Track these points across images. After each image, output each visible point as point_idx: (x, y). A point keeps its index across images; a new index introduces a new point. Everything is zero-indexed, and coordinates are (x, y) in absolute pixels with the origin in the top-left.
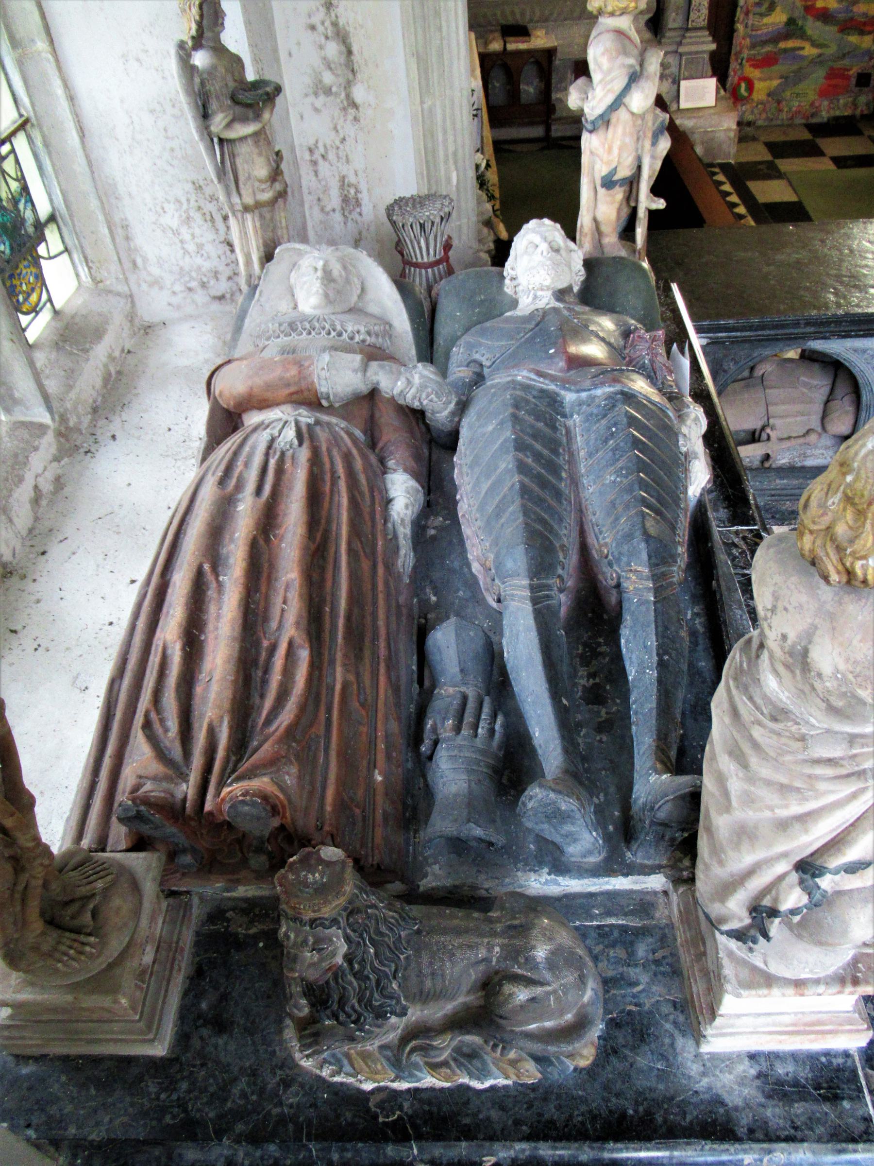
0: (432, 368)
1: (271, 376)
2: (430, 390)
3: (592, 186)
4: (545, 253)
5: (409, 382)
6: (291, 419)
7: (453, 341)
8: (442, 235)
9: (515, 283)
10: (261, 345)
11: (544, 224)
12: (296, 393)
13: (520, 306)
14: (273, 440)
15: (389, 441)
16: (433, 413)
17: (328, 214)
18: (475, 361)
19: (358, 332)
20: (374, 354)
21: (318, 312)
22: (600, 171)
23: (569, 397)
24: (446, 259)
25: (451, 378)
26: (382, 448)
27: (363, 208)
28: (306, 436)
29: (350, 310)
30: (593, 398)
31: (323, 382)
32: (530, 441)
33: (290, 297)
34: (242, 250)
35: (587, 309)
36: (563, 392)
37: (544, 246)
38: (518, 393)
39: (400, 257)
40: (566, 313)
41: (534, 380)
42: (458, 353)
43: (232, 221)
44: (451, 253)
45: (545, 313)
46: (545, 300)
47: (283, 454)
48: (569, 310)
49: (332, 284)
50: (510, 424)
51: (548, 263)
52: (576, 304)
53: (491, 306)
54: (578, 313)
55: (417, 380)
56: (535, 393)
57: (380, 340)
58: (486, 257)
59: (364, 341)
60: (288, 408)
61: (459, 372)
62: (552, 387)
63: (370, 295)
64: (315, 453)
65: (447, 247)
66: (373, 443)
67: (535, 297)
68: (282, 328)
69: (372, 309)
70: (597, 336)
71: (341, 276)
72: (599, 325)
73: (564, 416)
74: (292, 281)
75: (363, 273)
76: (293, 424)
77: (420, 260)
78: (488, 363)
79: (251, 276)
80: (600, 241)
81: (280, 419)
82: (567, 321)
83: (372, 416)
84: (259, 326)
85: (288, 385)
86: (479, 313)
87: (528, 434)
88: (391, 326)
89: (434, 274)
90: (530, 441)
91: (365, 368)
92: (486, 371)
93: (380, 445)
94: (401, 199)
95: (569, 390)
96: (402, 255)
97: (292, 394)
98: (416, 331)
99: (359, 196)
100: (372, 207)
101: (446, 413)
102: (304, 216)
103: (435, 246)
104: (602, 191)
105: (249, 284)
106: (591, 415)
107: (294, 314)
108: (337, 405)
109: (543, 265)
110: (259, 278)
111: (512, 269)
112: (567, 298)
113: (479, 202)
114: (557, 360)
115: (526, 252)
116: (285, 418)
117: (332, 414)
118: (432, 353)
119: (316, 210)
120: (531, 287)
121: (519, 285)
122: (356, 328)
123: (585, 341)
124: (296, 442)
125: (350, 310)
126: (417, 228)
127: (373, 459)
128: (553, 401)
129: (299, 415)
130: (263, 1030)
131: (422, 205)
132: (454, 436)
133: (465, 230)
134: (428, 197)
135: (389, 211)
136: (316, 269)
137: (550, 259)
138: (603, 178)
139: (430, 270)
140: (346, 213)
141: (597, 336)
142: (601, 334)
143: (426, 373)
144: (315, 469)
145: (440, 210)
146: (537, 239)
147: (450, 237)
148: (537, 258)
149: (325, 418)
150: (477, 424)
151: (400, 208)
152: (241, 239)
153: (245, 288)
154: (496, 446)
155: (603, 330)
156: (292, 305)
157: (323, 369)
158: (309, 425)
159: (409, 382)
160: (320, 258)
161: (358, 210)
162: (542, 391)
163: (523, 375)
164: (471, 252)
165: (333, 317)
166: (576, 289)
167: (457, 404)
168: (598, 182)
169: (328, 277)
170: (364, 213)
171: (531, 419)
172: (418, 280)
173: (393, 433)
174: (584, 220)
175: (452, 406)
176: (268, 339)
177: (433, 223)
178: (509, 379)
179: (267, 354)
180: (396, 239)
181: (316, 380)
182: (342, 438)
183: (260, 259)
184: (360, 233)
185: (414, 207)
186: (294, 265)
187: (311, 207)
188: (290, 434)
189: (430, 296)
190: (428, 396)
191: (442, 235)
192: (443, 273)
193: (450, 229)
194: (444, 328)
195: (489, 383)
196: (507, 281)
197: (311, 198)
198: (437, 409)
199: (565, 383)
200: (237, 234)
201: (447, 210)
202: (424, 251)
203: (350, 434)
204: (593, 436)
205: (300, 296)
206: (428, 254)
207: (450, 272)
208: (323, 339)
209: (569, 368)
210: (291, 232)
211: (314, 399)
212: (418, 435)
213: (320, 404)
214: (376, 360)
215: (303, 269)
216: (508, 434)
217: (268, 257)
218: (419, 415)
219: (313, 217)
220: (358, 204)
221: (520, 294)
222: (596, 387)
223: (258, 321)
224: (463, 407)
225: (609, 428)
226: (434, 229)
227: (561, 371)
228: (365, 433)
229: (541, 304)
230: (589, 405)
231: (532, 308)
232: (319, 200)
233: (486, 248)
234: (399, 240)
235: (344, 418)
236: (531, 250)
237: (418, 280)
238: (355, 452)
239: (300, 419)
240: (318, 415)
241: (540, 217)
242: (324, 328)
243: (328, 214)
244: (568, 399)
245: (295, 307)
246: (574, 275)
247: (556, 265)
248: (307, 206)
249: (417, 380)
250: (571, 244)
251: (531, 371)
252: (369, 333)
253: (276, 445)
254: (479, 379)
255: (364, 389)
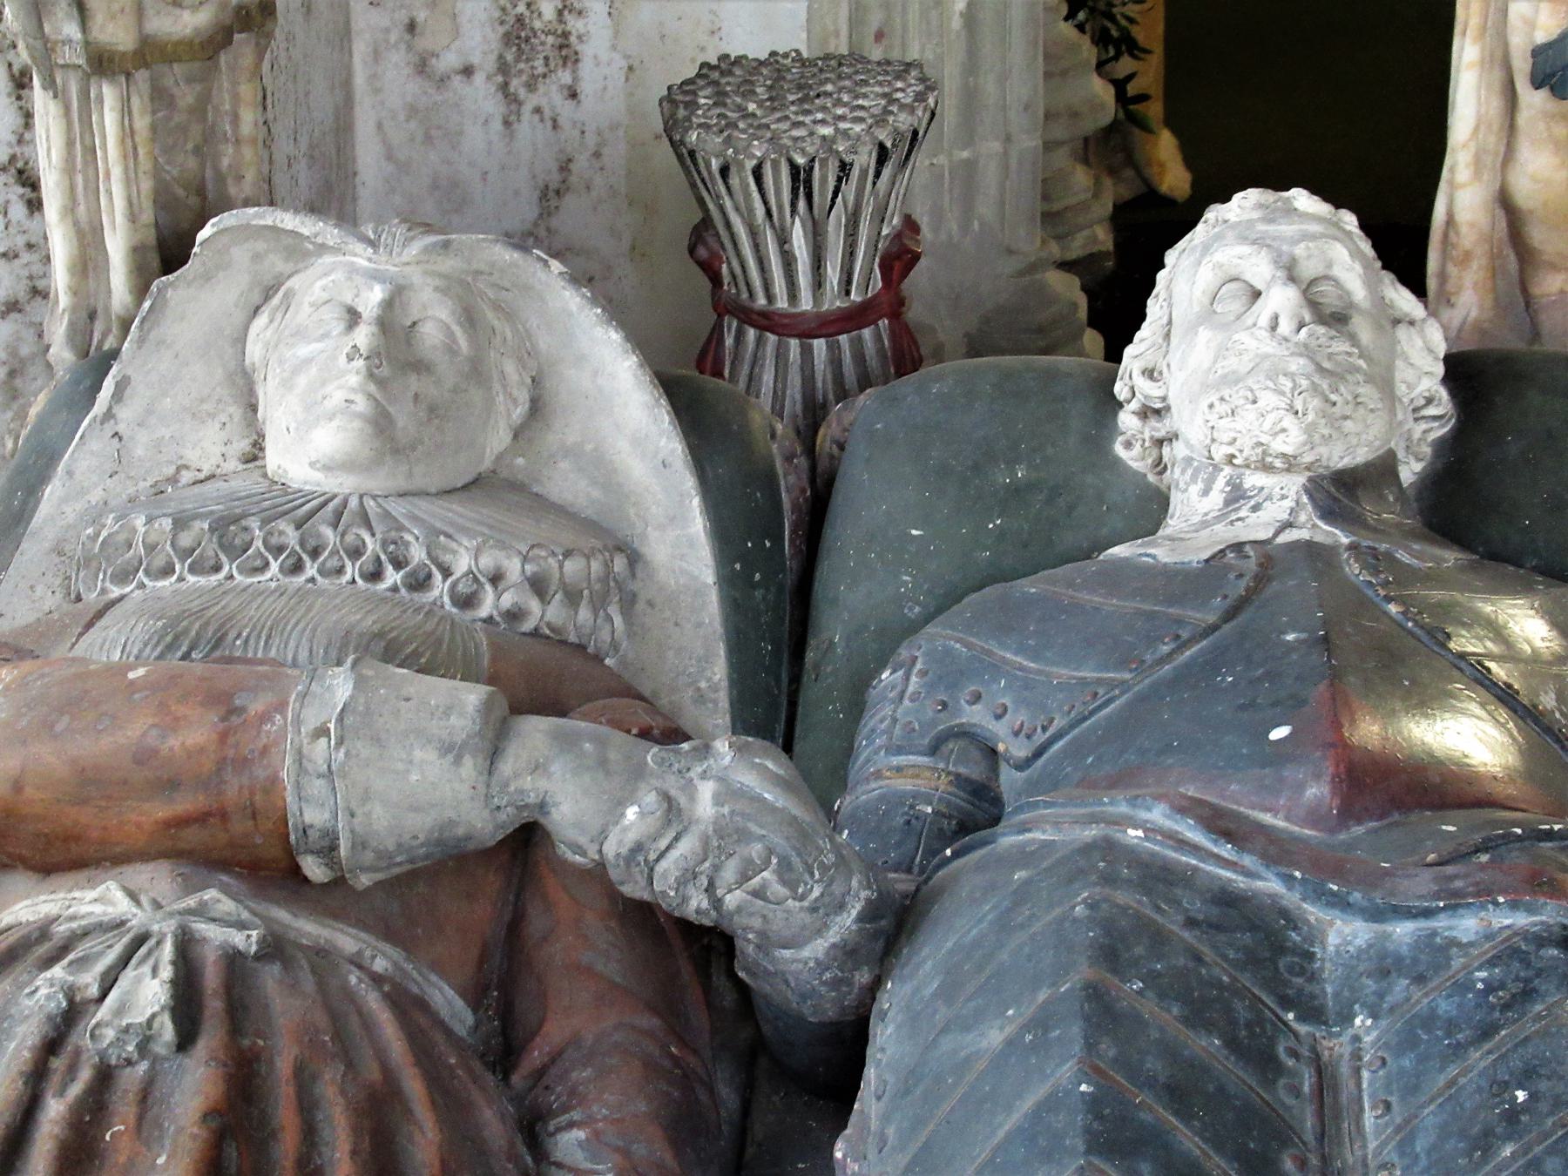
0: (774, 763)
1: (106, 742)
2: (756, 850)
3: (1498, 75)
4: (1285, 327)
5: (673, 812)
6: (166, 928)
7: (887, 642)
8: (880, 217)
9: (1160, 428)
10: (91, 597)
11: (1291, 211)
12: (202, 818)
13: (1174, 524)
14: (72, 1013)
15: (575, 1041)
16: (766, 942)
17: (443, 81)
18: (963, 732)
19: (496, 579)
20: (543, 680)
21: (341, 484)
22: (1531, 25)
23: (1342, 934)
24: (890, 304)
25: (860, 796)
26: (540, 1073)
27: (586, 67)
28: (214, 1005)
29: (477, 486)
30: (1437, 951)
31: (317, 787)
32: (1154, 1111)
33: (236, 411)
34: (70, 209)
35: (1451, 557)
36: (1313, 912)
37: (1282, 299)
38: (1122, 897)
39: (705, 283)
40: (1353, 570)
41: (1195, 849)
42: (900, 695)
43: (39, 97)
44: (918, 281)
45: (1270, 562)
46: (1276, 511)
47: (105, 1076)
48: (1374, 560)
49: (414, 382)
50: (1076, 1030)
51: (1298, 364)
52: (1414, 535)
53: (1061, 503)
54: (1406, 576)
55: (705, 803)
56: (1197, 907)
57: (584, 614)
58: (1069, 290)
59: (514, 615)
60: (156, 878)
61: (895, 771)
62: (1270, 885)
63: (565, 431)
64: (243, 1084)
65: (899, 259)
66: (504, 1048)
67: (1236, 495)
68: (186, 540)
69: (567, 485)
70: (1482, 680)
71: (451, 349)
72: (1498, 632)
73: (1313, 1013)
74: (254, 351)
75: (544, 342)
76: (168, 950)
77: (782, 303)
78: (1020, 750)
79: (92, 316)
80: (1525, 290)
81: (120, 924)
82: (1361, 604)
83: (515, 926)
84: (96, 520)
85: (170, 785)
86: (1001, 533)
87: (1150, 1083)
88: (634, 559)
89: (835, 362)
90: (1154, 1111)
91: (494, 743)
92: (1009, 779)
93: (536, 1056)
94: (728, 64)
95: (1341, 903)
96: (716, 280)
97: (182, 822)
98: (734, 583)
99: (574, 24)
100: (615, 71)
101: (817, 948)
102: (347, 84)
103: (850, 254)
104: (1534, 101)
105: (81, 337)
106: (1429, 1020)
107: (245, 483)
108: (365, 880)
109: (1273, 375)
110: (126, 325)
111: (1150, 374)
112: (1368, 508)
113: (1055, 69)
114: (1292, 773)
115: (1209, 313)
116: (138, 917)
117: (337, 915)
118: (796, 679)
119: (397, 65)
120: (1219, 453)
121: (1172, 437)
122: (487, 561)
123: (1427, 700)
124: (167, 1031)
125: (477, 486)
126: (780, 183)
127: (493, 1123)
128: (1270, 947)
129: (201, 912)
130: (1387, 1125)
131: (808, 96)
132: (848, 1043)
133: (990, 176)
134: (831, 64)
135: (678, 101)
136: (353, 317)
137: (1307, 351)
138: (1538, 52)
139: (819, 345)
140: (516, 84)
141: (1482, 680)
142: (1498, 671)
143: (747, 778)
144: (231, 1152)
145: (880, 121)
146: (1259, 269)
147: (911, 225)
148: (1254, 342)
149: (308, 928)
150: (943, 1013)
151: (720, 97)
152: (69, 169)
153: (61, 353)
154: (1008, 1123)
155: (1510, 654)
156: (244, 445)
157: (322, 732)
158: (233, 959)
159: (673, 812)
160: (376, 276)
161: (565, 77)
162: (1227, 899)
163: (1149, 823)
164: (1010, 266)
165: (398, 509)
166: (1410, 471)
167: (871, 913)
168: (1522, 66)
169: (395, 349)
170: (587, 88)
171: (1164, 1017)
172: (768, 378)
173: (590, 1015)
174: (1461, 199)
175: (846, 922)
176: (123, 577)
177: (845, 168)
178: (1091, 833)
179: (108, 645)
180: (697, 216)
181: (286, 775)
182: (368, 1025)
183: (137, 251)
184: (565, 167)
185: (775, 101)
186: (268, 293)
187: (377, 55)
188: (148, 992)
189: (810, 451)
190: (744, 878)
191: (880, 217)
192: (873, 362)
193: (920, 189)
194: (851, 594)
195: (1007, 840)
196: (1127, 420)
197: (379, 18)
198: (778, 925)
199: (1327, 873)
200: (57, 155)
201: (904, 121)
202: (800, 266)
203: (407, 1005)
204: (1430, 1117)
205: (279, 413)
206: (818, 283)
207: (906, 357)
208: (342, 597)
209: (1349, 812)
210: (283, 148)
211: (275, 852)
212: (700, 1019)
213: (296, 871)
214: (555, 707)
215: (302, 313)
216: (1065, 1074)
217: (168, 251)
218: (711, 945)
219: (383, 91)
220: (566, 51)
221: (1175, 474)
222: (1456, 902)
223: (96, 496)
224: (894, 926)
225: (1506, 1087)
226: (849, 190)
227: (1314, 818)
228: (475, 998)
229: (1257, 526)
230: (1420, 979)
231: (1224, 534)
232: (412, 27)
233: (1077, 248)
234: (706, 223)
235: (389, 934)
236: (1230, 306)
237: (768, 378)
238: (414, 1086)
239: (201, 927)
240: (282, 915)
241: (1279, 182)
242: (356, 552)
243: (443, 81)
244: (1333, 940)
245: (254, 455)
246: (1408, 404)
247: (1330, 373)
248: (360, 49)
249: (705, 803)
250: (1404, 299)
251: (1186, 808)
252: (538, 586)
253: (81, 1038)
254: (977, 812)
255: (482, 822)
